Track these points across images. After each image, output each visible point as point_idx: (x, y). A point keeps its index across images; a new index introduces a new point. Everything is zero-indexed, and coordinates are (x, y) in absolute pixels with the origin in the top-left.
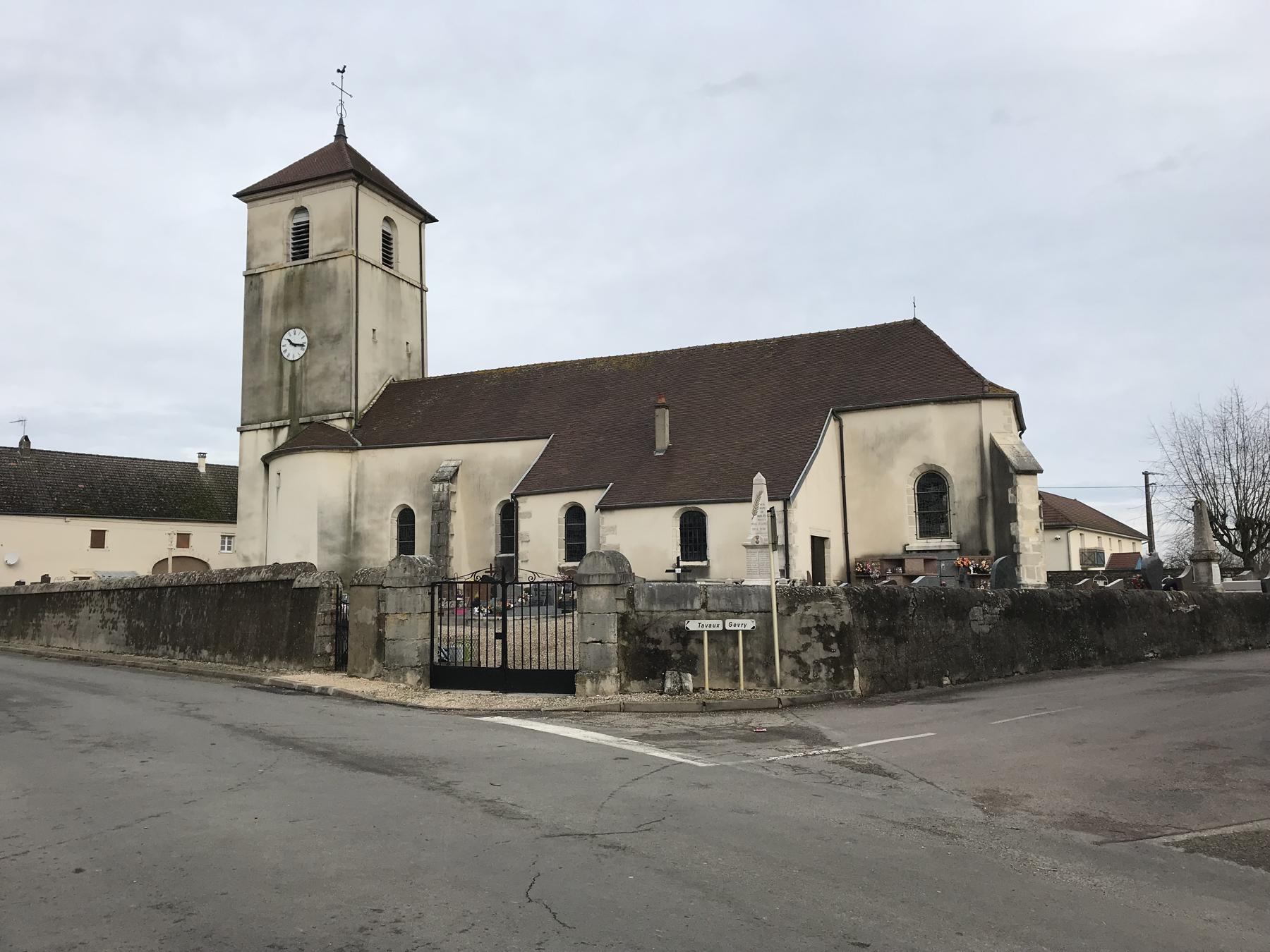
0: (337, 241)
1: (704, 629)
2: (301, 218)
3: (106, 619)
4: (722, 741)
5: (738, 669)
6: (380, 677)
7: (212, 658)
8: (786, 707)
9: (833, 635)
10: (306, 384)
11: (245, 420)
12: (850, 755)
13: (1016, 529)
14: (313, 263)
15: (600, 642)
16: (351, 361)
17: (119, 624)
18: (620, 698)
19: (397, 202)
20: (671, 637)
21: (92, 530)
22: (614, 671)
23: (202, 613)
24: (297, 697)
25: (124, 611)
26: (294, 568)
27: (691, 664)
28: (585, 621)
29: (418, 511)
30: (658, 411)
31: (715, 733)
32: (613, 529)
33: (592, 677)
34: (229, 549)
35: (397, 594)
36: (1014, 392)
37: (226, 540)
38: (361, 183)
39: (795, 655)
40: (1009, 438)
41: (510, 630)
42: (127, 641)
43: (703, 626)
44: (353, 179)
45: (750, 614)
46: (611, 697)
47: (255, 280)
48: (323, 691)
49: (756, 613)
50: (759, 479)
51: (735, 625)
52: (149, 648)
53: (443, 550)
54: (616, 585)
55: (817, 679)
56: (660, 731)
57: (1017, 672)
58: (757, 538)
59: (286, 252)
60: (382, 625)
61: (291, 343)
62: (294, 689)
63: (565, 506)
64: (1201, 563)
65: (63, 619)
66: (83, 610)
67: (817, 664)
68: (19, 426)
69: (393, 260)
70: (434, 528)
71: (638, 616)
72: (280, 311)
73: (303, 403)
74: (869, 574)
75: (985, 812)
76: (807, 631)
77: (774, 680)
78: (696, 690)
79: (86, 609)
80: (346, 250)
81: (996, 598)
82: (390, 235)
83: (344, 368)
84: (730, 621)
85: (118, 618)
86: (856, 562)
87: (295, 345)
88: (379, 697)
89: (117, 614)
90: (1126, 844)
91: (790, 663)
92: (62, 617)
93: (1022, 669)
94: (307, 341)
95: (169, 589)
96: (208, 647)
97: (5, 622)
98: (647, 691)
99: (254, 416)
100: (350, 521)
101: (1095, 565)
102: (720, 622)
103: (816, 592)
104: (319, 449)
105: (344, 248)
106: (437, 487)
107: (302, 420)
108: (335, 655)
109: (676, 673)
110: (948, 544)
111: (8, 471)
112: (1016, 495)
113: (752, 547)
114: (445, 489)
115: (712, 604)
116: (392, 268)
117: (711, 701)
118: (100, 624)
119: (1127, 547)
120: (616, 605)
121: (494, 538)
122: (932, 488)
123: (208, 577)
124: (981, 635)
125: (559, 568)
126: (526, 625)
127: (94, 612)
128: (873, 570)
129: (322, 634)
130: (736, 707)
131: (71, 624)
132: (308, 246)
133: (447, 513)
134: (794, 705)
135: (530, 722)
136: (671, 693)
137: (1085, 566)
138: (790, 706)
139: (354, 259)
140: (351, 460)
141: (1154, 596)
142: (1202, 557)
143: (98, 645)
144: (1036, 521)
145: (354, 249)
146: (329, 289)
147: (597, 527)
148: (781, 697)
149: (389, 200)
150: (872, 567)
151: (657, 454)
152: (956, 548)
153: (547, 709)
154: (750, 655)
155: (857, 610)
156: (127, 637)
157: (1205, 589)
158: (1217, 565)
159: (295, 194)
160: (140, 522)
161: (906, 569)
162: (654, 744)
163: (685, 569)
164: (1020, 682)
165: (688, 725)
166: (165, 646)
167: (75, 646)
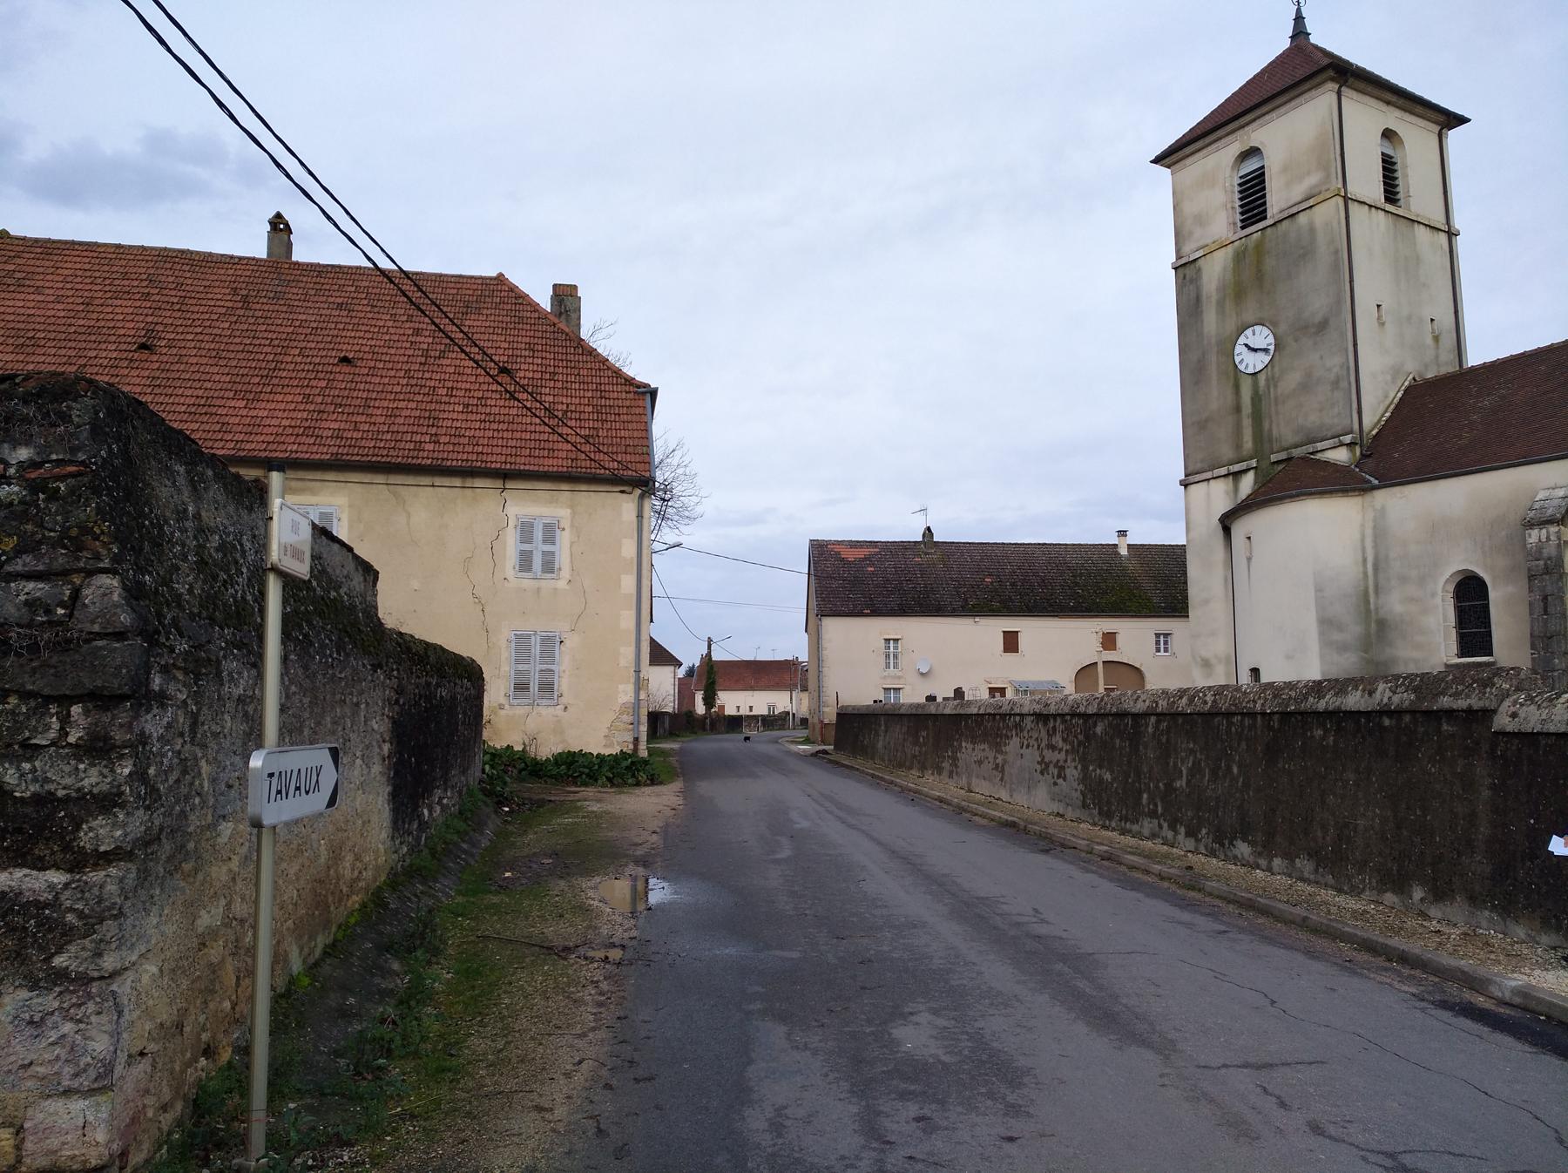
0: (1313, 180)
2: (1251, 165)
3: (1046, 760)
7: (1263, 862)
10: (1276, 405)
11: (1190, 469)
16: (1348, 359)
17: (1068, 771)
23: (1229, 768)
25: (1073, 751)
34: (1166, 650)
37: (1162, 638)
44: (1333, 80)
47: (1189, 271)
52: (1125, 819)
59: (1231, 220)
69: (1401, 196)
72: (1229, 305)
73: (1275, 433)
79: (1015, 742)
82: (1391, 157)
85: (1066, 761)
92: (982, 750)
95: (1153, 719)
100: (1367, 602)
105: (1324, 188)
106: (1534, 536)
107: (1274, 458)
118: (1038, 768)
127: (1028, 746)
139: (1340, 201)
140: (1363, 507)
145: (1340, 185)
149: (1388, 103)
159: (1240, 132)
160: (1056, 619)
167: (1004, 795)
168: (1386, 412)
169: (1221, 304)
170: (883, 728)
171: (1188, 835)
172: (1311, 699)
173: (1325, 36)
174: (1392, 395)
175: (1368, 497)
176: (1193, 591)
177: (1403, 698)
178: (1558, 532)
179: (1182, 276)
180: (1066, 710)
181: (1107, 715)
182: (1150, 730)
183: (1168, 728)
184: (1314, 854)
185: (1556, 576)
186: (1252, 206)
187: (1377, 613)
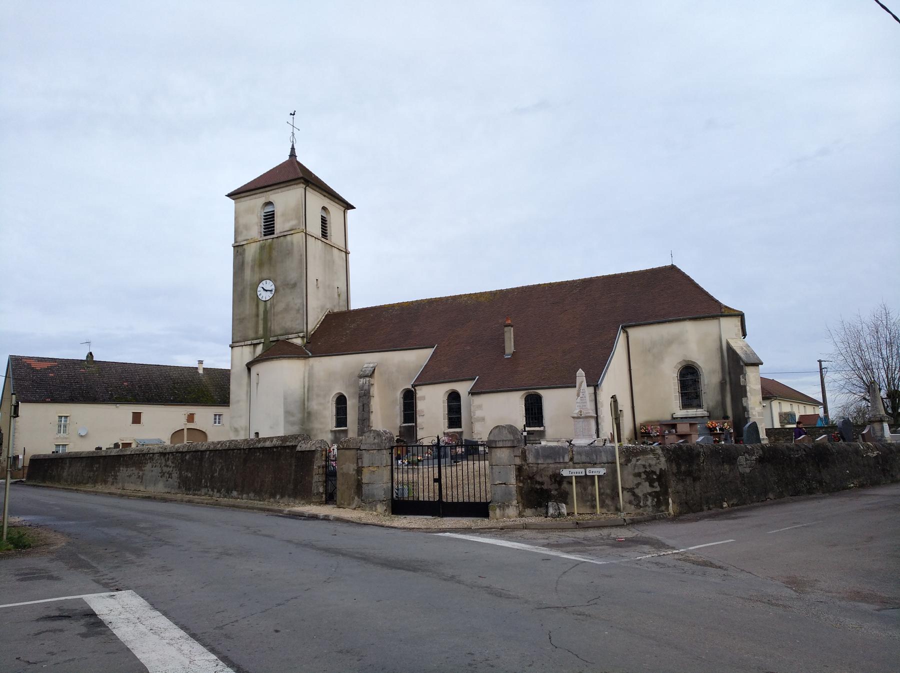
0: (292, 223)
1: (573, 474)
2: (269, 209)
3: (164, 471)
4: (600, 547)
5: (595, 500)
6: (359, 507)
7: (240, 497)
8: (629, 524)
9: (655, 477)
10: (274, 315)
11: (235, 340)
12: (687, 555)
13: (747, 402)
14: (277, 237)
15: (505, 484)
18: (520, 521)
19: (330, 196)
20: (551, 480)
21: (133, 412)
22: (515, 502)
23: (232, 467)
24: (307, 522)
26: (296, 438)
27: (564, 497)
28: (494, 471)
29: (349, 397)
30: (506, 329)
31: (592, 542)
32: (480, 407)
33: (500, 507)
34: (219, 423)
35: (369, 454)
36: (742, 312)
37: (217, 417)
38: (308, 186)
39: (631, 491)
40: (739, 342)
41: (443, 477)
42: (179, 486)
43: (577, 473)
44: (303, 183)
45: (602, 464)
46: (514, 519)
47: (240, 249)
48: (326, 518)
49: (605, 463)
50: (581, 373)
51: (593, 472)
53: (366, 422)
54: (514, 447)
55: (646, 506)
56: (557, 542)
57: (769, 498)
58: (581, 412)
59: (260, 231)
60: (360, 474)
61: (264, 290)
62: (305, 517)
63: (447, 392)
64: (876, 423)
65: (134, 472)
66: (147, 465)
67: (645, 496)
68: (86, 346)
69: (328, 235)
71: (529, 467)
72: (257, 269)
73: (272, 328)
74: (650, 433)
75: (795, 591)
76: (638, 475)
77: (619, 507)
78: (568, 514)
80: (299, 228)
81: (752, 449)
82: (325, 218)
84: (590, 469)
85: (173, 471)
86: (641, 426)
87: (266, 291)
88: (364, 521)
89: (171, 468)
90: (893, 610)
91: (628, 495)
92: (133, 470)
93: (771, 496)
94: (274, 288)
95: (208, 452)
96: (237, 489)
97: (92, 473)
98: (536, 515)
99: (240, 337)
100: (304, 404)
101: (789, 423)
102: (583, 470)
103: (643, 449)
105: (298, 227)
106: (362, 381)
107: (271, 339)
108: (326, 494)
109: (555, 503)
110: (701, 413)
111: (79, 375)
112: (745, 380)
113: (578, 418)
115: (576, 458)
116: (327, 239)
117: (581, 522)
118: (160, 475)
119: (810, 411)
120: (514, 460)
122: (689, 376)
123: (235, 444)
124: (745, 475)
125: (444, 433)
126: (426, 470)
127: (155, 466)
128: (652, 431)
129: (317, 480)
130: (598, 525)
131: (139, 475)
132: (274, 227)
133: (369, 398)
134: (634, 523)
135: (471, 537)
136: (553, 516)
137: (783, 424)
138: (631, 523)
139: (304, 234)
141: (852, 447)
142: (877, 419)
143: (160, 488)
144: (759, 397)
145: (304, 228)
146: (288, 254)
147: (469, 405)
148: (624, 518)
149: (325, 196)
150: (652, 429)
151: (506, 357)
152: (706, 415)
153: (475, 527)
154: (602, 491)
155: (669, 460)
156: (179, 483)
157: (880, 440)
158: (887, 424)
159: (265, 193)
160: (163, 406)
161: (678, 430)
162: (559, 550)
163: (529, 433)
164: (771, 505)
165: (572, 537)
166: (207, 489)
167: (142, 488)
168: (317, 324)
170: (68, 465)
171: (217, 492)
172: (257, 444)
173: (302, 158)
175: (307, 361)
176: (232, 396)
177: (279, 443)
178: (369, 380)
179: (236, 251)
180: (174, 451)
181: (190, 452)
182: (207, 456)
183: (213, 455)
184: (255, 492)
185: (367, 397)
186: (268, 226)
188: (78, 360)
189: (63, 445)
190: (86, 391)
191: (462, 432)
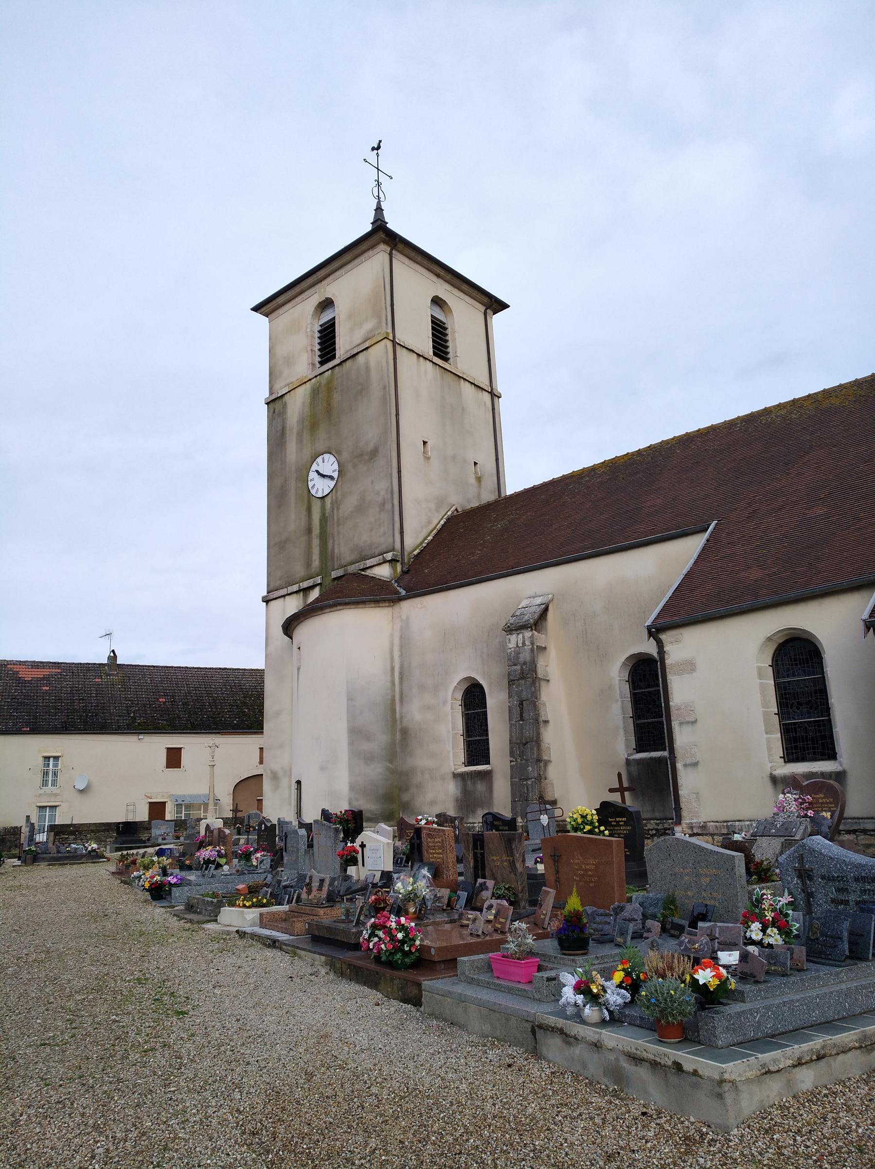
0: (369, 325)
2: (326, 317)
10: (338, 526)
11: (272, 586)
21: (168, 748)
47: (278, 406)
53: (532, 749)
63: (769, 639)
69: (450, 356)
70: (514, 711)
72: (306, 436)
73: (336, 551)
82: (444, 324)
83: (382, 493)
87: (323, 476)
99: (280, 579)
100: (394, 711)
104: (346, 604)
106: (514, 640)
107: (334, 574)
114: (527, 643)
121: (622, 726)
125: (774, 780)
139: (390, 345)
145: (390, 331)
149: (438, 276)
159: (319, 285)
160: (218, 735)
168: (429, 535)
169: (300, 435)
174: (435, 522)
175: (397, 608)
187: (401, 722)
188: (95, 664)
189: (50, 807)
190: (93, 713)
191: (840, 776)
